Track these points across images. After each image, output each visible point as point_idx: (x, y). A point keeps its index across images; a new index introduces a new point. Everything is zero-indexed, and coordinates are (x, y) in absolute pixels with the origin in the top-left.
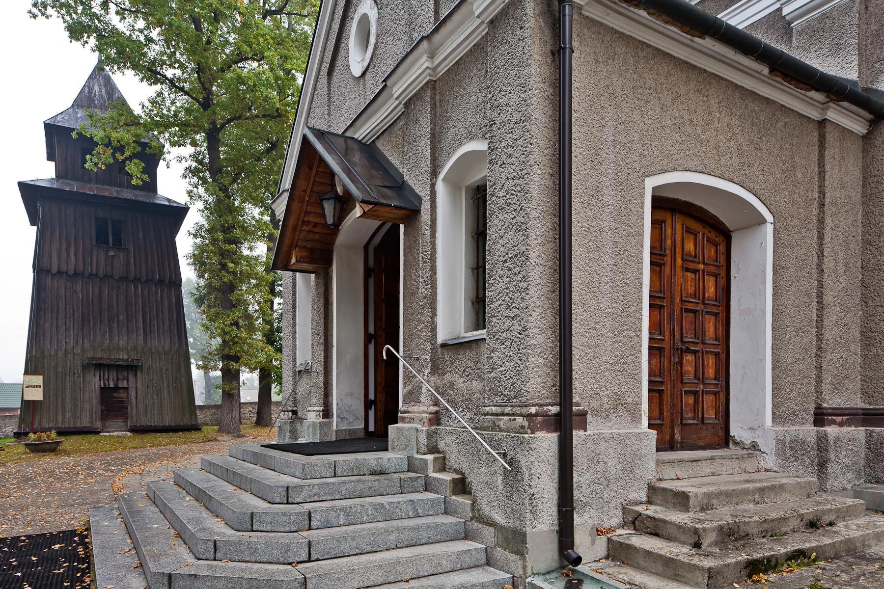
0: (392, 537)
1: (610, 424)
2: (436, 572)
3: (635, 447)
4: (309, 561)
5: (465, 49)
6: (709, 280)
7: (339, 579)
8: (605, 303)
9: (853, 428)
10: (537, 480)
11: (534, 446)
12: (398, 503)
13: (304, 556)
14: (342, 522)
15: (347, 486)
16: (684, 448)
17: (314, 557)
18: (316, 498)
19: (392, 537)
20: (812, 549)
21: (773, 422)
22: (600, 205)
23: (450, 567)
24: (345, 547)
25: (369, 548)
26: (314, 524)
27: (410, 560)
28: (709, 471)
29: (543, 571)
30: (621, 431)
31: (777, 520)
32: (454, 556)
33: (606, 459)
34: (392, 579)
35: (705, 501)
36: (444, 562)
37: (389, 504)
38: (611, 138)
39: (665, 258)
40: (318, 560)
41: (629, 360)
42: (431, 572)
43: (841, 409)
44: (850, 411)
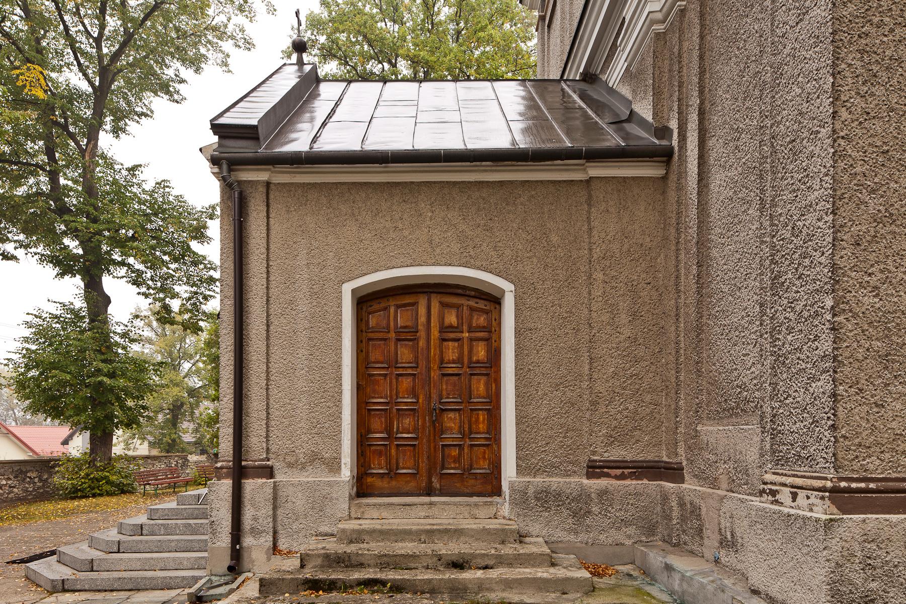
0: (173, 544)
1: (305, 474)
2: (178, 568)
3: (324, 493)
4: (119, 552)
5: (395, 167)
6: (478, 346)
7: (112, 563)
8: (301, 384)
9: (645, 481)
10: (217, 512)
11: (214, 489)
12: (202, 524)
13: (115, 549)
14: (162, 533)
15: (187, 511)
16: (441, 494)
17: (121, 550)
18: (166, 517)
19: (173, 544)
20: (389, 580)
21: (517, 473)
22: (294, 313)
23: (190, 566)
24: (141, 547)
25: (157, 549)
26: (144, 532)
27: (174, 559)
28: (423, 514)
29: (221, 574)
30: (309, 479)
31: (402, 555)
32: (192, 560)
33: (294, 500)
34: (147, 568)
35: (355, 536)
36: (185, 563)
37: (195, 524)
38: (305, 263)
39: (418, 334)
40: (124, 552)
41: (327, 425)
42: (176, 567)
43: (626, 461)
44: (636, 464)
